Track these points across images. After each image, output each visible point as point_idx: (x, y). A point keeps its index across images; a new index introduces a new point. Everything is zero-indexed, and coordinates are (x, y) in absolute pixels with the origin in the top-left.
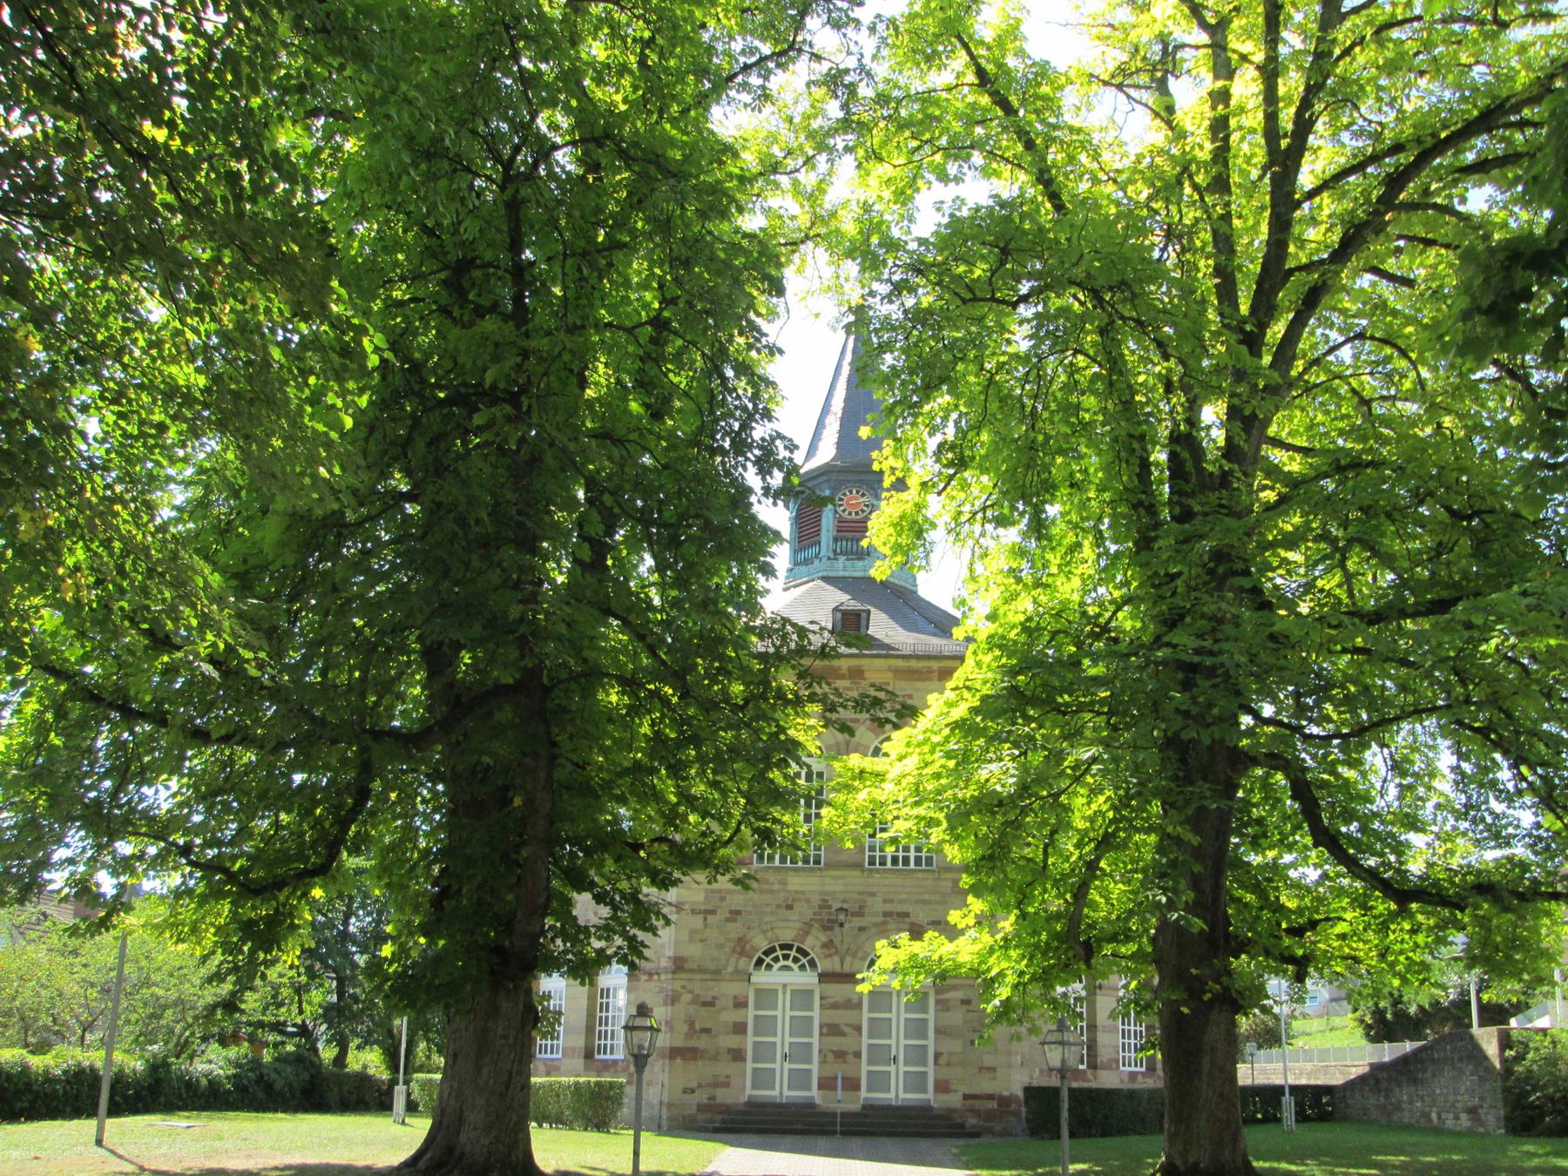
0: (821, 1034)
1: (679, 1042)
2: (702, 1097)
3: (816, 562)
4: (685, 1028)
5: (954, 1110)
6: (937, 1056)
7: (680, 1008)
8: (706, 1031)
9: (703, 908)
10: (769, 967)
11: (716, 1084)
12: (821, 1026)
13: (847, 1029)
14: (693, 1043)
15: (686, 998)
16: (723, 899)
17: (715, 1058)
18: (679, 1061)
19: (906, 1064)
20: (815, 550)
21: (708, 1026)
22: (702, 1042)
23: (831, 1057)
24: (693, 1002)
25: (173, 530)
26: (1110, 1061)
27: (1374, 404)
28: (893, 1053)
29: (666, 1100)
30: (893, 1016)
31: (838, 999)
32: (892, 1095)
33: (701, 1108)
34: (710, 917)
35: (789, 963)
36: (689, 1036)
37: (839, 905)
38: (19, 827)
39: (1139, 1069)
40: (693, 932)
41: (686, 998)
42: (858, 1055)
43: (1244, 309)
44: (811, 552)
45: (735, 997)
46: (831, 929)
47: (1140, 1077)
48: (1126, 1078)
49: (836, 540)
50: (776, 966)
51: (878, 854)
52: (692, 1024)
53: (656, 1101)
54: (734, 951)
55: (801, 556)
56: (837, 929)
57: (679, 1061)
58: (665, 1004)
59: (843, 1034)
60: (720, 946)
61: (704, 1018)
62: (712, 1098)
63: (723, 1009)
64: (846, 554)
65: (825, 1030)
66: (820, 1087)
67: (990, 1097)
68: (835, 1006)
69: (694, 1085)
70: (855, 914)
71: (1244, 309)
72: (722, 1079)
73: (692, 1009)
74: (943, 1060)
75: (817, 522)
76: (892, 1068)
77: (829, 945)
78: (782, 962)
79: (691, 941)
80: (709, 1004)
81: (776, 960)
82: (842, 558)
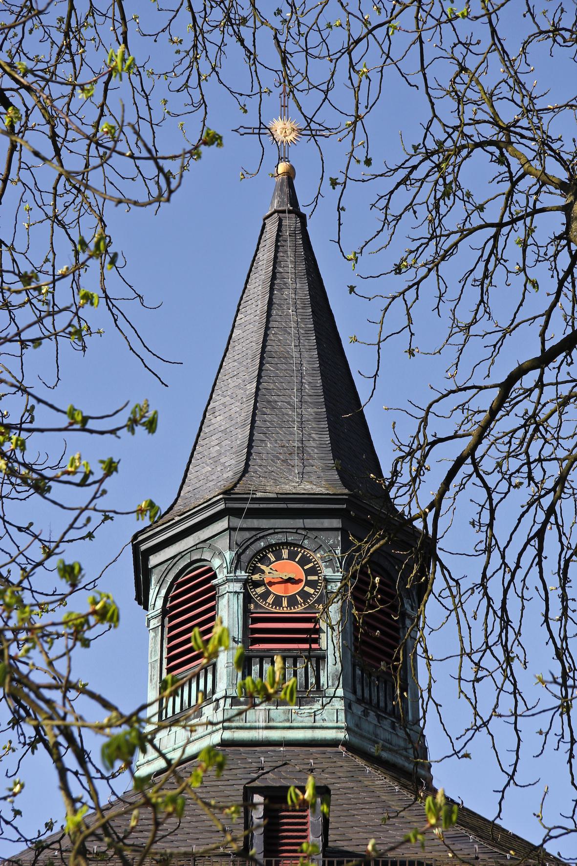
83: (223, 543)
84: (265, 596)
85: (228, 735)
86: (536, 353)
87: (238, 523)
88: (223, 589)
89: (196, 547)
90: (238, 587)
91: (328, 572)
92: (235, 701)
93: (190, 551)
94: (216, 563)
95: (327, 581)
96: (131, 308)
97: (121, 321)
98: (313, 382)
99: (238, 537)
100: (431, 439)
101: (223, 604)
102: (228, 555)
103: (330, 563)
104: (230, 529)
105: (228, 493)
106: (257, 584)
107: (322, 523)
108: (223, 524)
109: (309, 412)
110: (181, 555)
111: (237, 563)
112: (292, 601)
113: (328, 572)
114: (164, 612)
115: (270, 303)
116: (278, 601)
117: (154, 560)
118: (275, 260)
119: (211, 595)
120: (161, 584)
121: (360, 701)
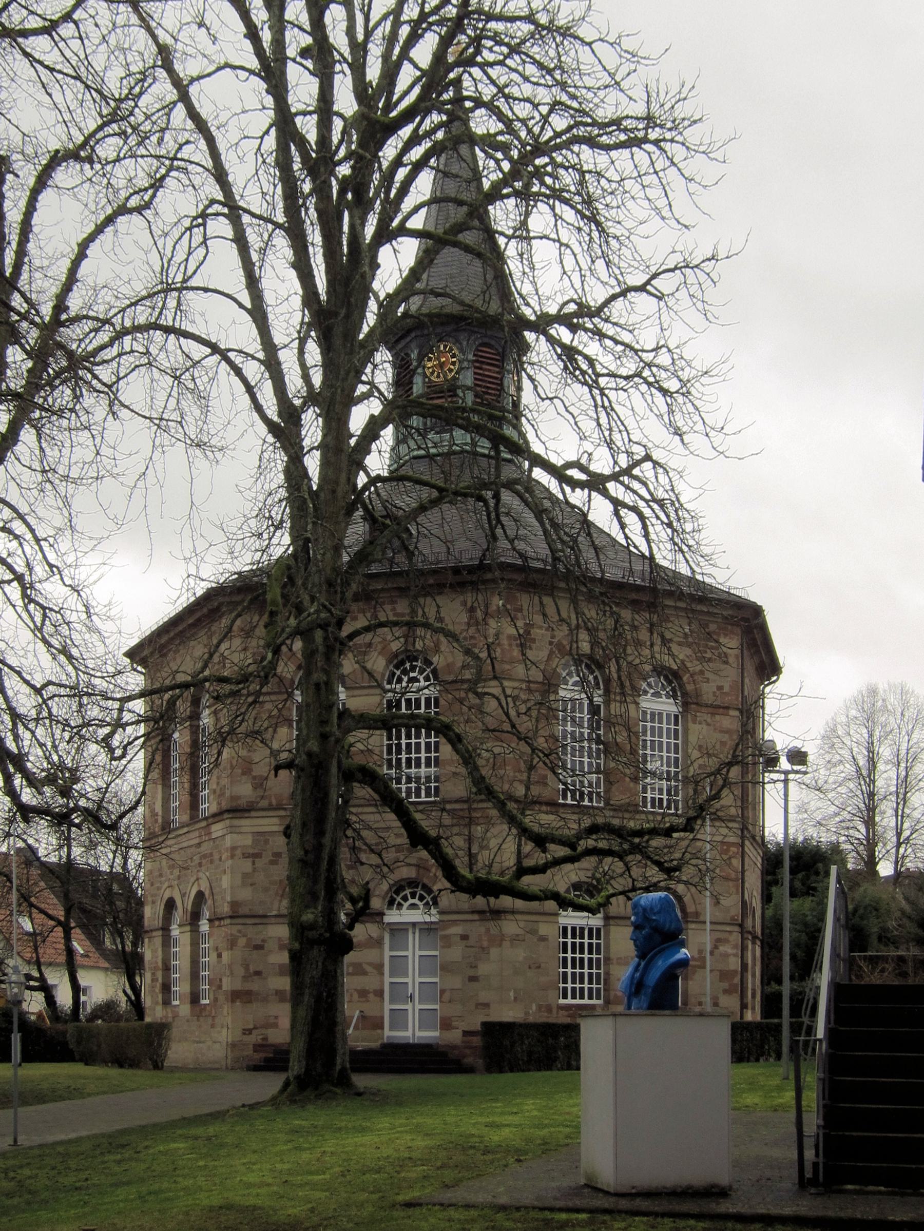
1: (238, 986)
2: (255, 1038)
5: (454, 1047)
8: (258, 973)
9: (251, 851)
10: (400, 906)
11: (267, 1026)
13: (369, 969)
14: (249, 986)
16: (266, 842)
17: (265, 1000)
19: (420, 1003)
22: (255, 985)
24: (247, 945)
25: (624, 123)
28: (410, 991)
29: (230, 1040)
30: (409, 953)
32: (409, 1034)
33: (257, 1048)
34: (257, 860)
35: (416, 901)
36: (246, 978)
38: (637, 692)
39: (594, 1002)
40: (245, 876)
41: (242, 941)
42: (380, 993)
43: (392, 196)
50: (406, 905)
52: (247, 967)
54: (277, 894)
59: (365, 973)
60: (266, 890)
62: (265, 1039)
69: (251, 1026)
71: (392, 196)
72: (272, 1020)
74: (447, 996)
76: (409, 1007)
78: (411, 901)
79: (244, 884)
81: (405, 899)
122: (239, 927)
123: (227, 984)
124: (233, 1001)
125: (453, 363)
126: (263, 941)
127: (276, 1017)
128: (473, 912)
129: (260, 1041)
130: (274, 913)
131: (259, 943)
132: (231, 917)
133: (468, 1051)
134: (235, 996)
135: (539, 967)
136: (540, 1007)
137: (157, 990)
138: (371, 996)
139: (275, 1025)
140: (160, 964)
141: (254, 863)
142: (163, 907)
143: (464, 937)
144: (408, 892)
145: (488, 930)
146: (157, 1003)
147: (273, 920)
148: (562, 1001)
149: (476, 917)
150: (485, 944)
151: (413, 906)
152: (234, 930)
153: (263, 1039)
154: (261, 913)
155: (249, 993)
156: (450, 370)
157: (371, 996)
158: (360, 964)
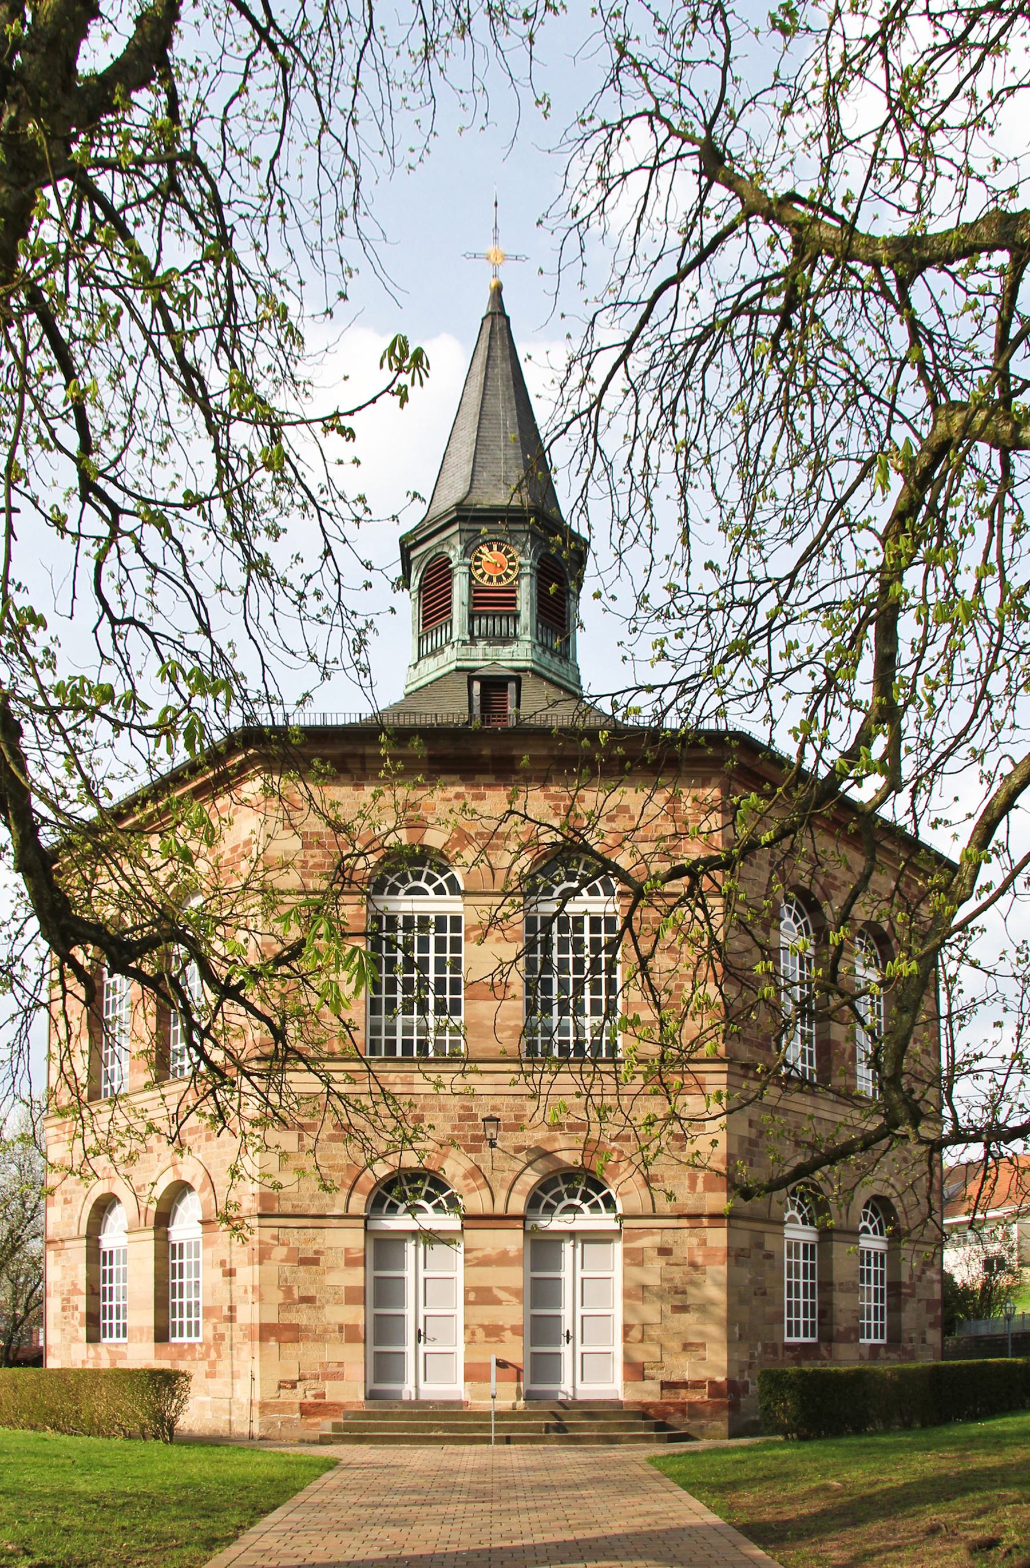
0: (467, 1303)
1: (272, 1318)
3: (448, 649)
4: (279, 1297)
6: (627, 1329)
7: (272, 1267)
11: (327, 1376)
12: (466, 1292)
13: (502, 1295)
15: (279, 1252)
17: (320, 1337)
18: (273, 1343)
20: (444, 634)
21: (311, 1293)
22: (302, 1317)
23: (480, 1334)
26: (849, 1330)
27: (511, 1042)
29: (257, 1398)
31: (489, 1251)
36: (284, 1307)
37: (486, 1115)
39: (878, 1341)
41: (280, 1252)
44: (439, 638)
45: (347, 1250)
46: (477, 1150)
47: (882, 1350)
48: (866, 1353)
49: (472, 617)
51: (383, 1037)
52: (288, 1291)
53: (245, 1400)
55: (427, 646)
56: (486, 1150)
57: (273, 1343)
58: (251, 1263)
59: (498, 1302)
61: (304, 1280)
63: (331, 1268)
64: (485, 637)
65: (472, 1296)
66: (467, 1378)
67: (697, 1385)
68: (485, 1262)
70: (509, 1128)
72: (333, 1368)
73: (287, 1268)
74: (636, 1334)
75: (447, 593)
77: (476, 1172)
78: (567, 1201)
80: (314, 1261)
81: (559, 1198)
82: (482, 644)
83: (456, 540)
84: (482, 576)
85: (460, 664)
86: (674, 272)
87: (466, 526)
88: (456, 571)
89: (440, 544)
90: (465, 569)
91: (521, 560)
92: (464, 643)
93: (435, 547)
94: (452, 554)
95: (521, 566)
96: (381, 247)
97: (368, 249)
98: (514, 434)
99: (465, 536)
100: (595, 348)
101: (456, 580)
102: (460, 548)
103: (522, 553)
104: (460, 531)
105: (459, 506)
106: (477, 568)
107: (520, 1193)
108: (456, 527)
109: (511, 452)
110: (430, 550)
111: (465, 553)
112: (499, 579)
113: (521, 560)
114: (420, 588)
115: (486, 377)
116: (490, 579)
117: (413, 555)
118: (490, 348)
119: (449, 575)
120: (418, 569)
121: (541, 644)
122: (275, 1231)
123: (249, 1314)
124: (262, 1339)
125: (512, 568)
126: (317, 1252)
127: (340, 1364)
128: (679, 1217)
129: (311, 1399)
130: (339, 1211)
131: (310, 1255)
132: (261, 1216)
133: (671, 1409)
134: (266, 1332)
135: (764, 1294)
136: (765, 1346)
137: (76, 1322)
138: (508, 1335)
139: (337, 1376)
140: (83, 1286)
141: (300, 1138)
142: (89, 1207)
143: (664, 1251)
144: (563, 1188)
145: (703, 1242)
146: (75, 1339)
147: (335, 1222)
148: (787, 1340)
149: (684, 1223)
150: (699, 1260)
151: (575, 1209)
152: (267, 1234)
153: (316, 1396)
154: (313, 1211)
155: (295, 1328)
156: (508, 576)
157: (508, 1335)
158: (489, 1290)
